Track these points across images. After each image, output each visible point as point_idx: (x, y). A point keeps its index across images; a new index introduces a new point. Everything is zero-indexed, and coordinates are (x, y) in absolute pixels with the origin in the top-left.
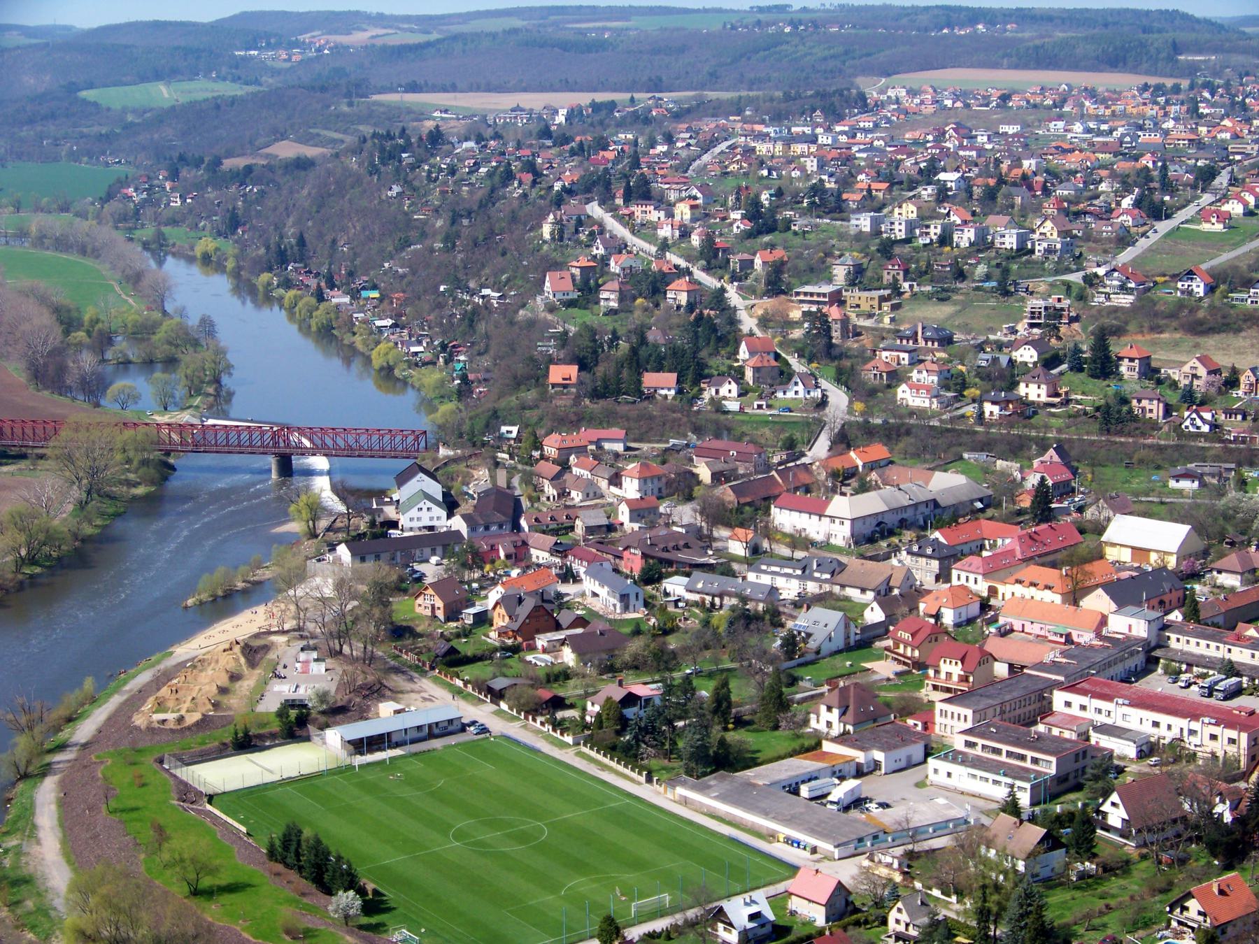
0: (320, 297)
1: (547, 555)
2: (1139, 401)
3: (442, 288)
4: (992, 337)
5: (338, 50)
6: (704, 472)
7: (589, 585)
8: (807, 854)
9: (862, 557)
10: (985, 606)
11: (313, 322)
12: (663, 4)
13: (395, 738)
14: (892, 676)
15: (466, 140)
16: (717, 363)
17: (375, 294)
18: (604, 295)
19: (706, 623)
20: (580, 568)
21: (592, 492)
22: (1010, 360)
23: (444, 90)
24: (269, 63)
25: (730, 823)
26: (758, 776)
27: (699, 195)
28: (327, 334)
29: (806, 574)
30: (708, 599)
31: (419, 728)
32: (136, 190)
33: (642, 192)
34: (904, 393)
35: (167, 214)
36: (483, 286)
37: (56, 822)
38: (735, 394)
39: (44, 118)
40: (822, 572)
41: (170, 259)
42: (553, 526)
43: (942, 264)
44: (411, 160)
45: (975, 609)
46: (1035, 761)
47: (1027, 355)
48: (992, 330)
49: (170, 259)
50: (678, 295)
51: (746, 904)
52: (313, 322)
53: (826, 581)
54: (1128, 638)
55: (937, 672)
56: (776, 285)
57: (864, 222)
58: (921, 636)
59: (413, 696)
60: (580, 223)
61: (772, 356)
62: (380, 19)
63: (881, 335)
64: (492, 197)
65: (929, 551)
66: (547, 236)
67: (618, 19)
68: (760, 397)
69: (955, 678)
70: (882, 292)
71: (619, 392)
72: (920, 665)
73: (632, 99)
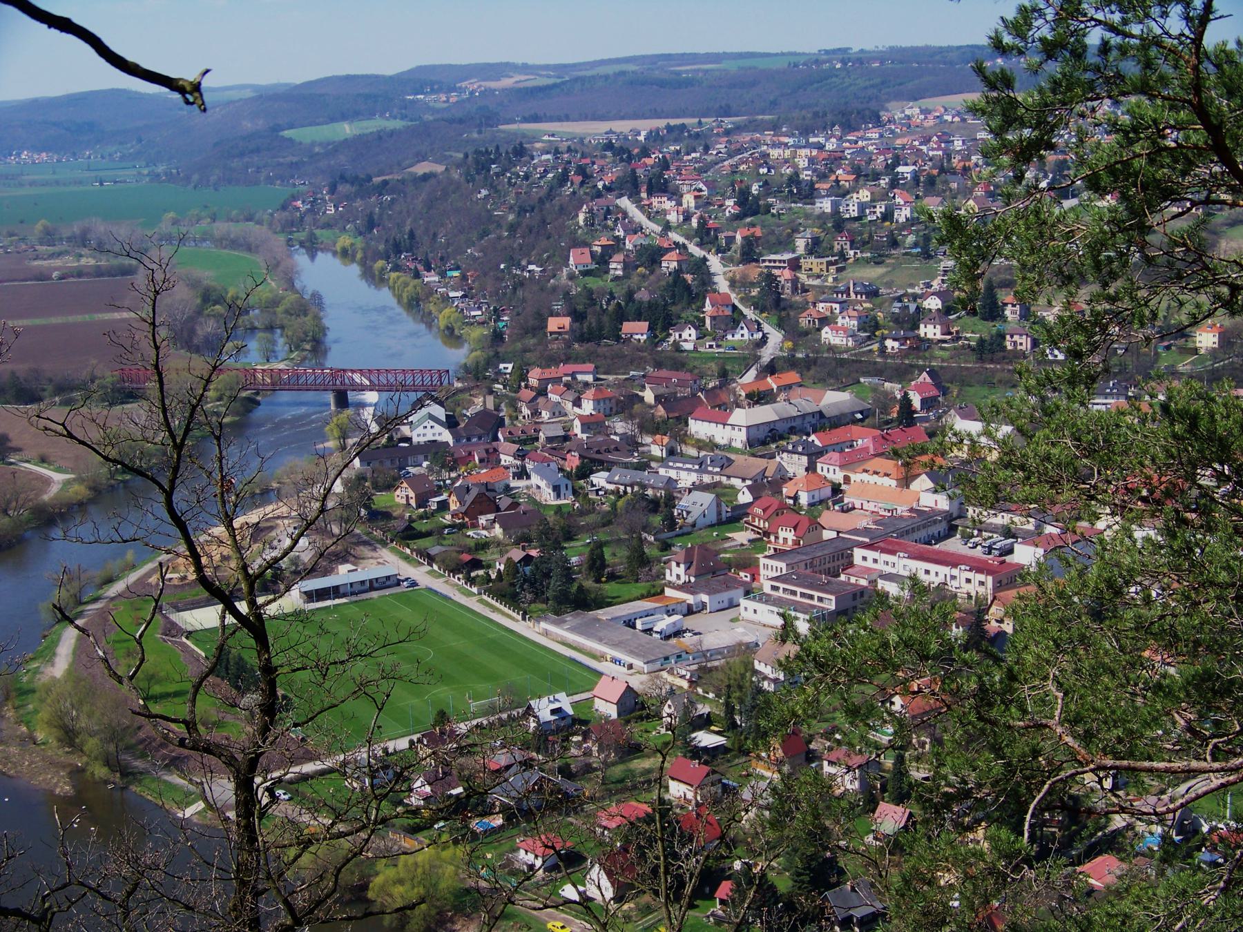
0: (417, 275)
1: (511, 459)
2: (1012, 337)
3: (502, 266)
4: (910, 291)
5: (490, 92)
6: (649, 396)
7: (535, 480)
8: (625, 670)
9: (754, 455)
10: (836, 490)
11: (405, 295)
12: (751, 50)
13: (342, 590)
14: (745, 542)
15: (548, 153)
16: (688, 314)
17: (456, 274)
18: (612, 266)
19: (614, 505)
20: (529, 466)
21: (558, 411)
22: (918, 308)
23: (559, 120)
24: (431, 104)
25: (575, 648)
26: (603, 614)
27: (704, 188)
28: (414, 304)
29: (702, 469)
30: (622, 488)
31: (363, 582)
32: (303, 202)
33: (659, 187)
34: (827, 335)
35: (323, 220)
36: (530, 263)
37: (71, 651)
38: (694, 337)
39: (252, 152)
40: (714, 467)
41: (319, 254)
42: (524, 437)
43: (881, 236)
44: (497, 170)
45: (827, 491)
46: (821, 599)
47: (933, 303)
48: (912, 286)
49: (319, 254)
50: (670, 263)
51: (550, 702)
52: (405, 295)
53: (717, 473)
54: (933, 510)
55: (777, 538)
56: (749, 254)
57: (826, 205)
58: (770, 511)
59: (371, 561)
60: (608, 212)
61: (730, 308)
62: (525, 68)
63: (822, 290)
64: (551, 194)
65: (800, 449)
66: (582, 223)
67: (711, 63)
68: (714, 339)
69: (790, 542)
70: (830, 258)
71: (601, 337)
72: (767, 534)
73: (700, 123)
